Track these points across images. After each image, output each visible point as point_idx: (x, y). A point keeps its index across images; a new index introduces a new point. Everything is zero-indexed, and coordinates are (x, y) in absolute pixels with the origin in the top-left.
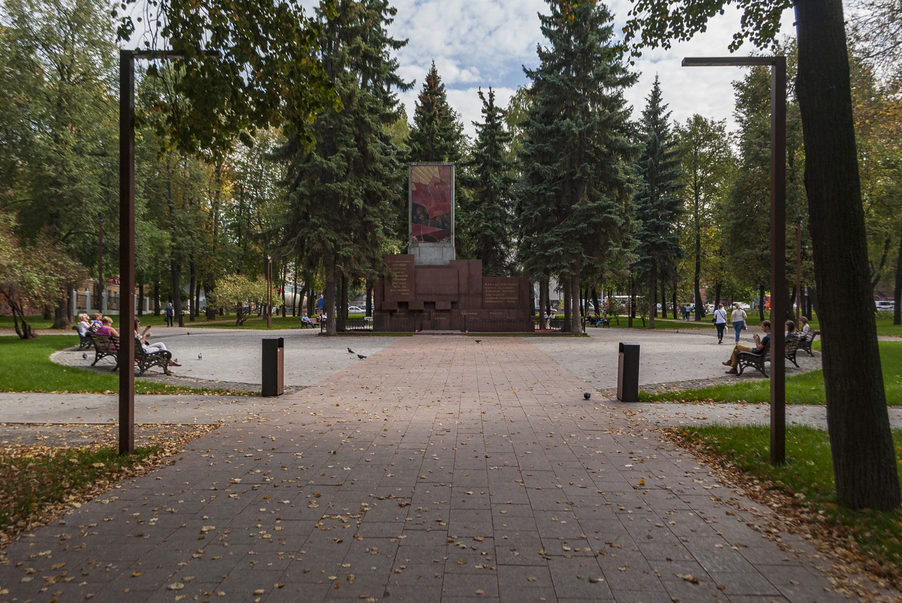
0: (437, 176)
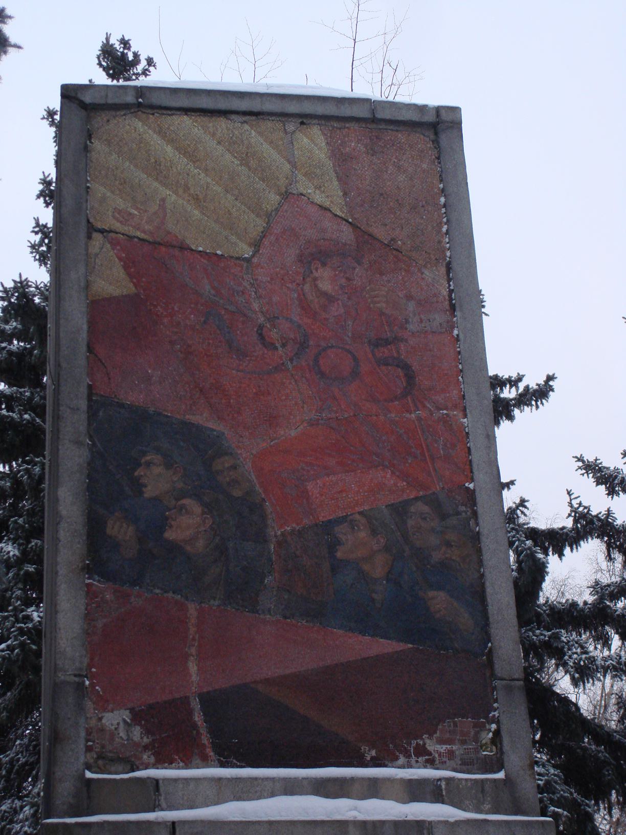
0: (327, 193)
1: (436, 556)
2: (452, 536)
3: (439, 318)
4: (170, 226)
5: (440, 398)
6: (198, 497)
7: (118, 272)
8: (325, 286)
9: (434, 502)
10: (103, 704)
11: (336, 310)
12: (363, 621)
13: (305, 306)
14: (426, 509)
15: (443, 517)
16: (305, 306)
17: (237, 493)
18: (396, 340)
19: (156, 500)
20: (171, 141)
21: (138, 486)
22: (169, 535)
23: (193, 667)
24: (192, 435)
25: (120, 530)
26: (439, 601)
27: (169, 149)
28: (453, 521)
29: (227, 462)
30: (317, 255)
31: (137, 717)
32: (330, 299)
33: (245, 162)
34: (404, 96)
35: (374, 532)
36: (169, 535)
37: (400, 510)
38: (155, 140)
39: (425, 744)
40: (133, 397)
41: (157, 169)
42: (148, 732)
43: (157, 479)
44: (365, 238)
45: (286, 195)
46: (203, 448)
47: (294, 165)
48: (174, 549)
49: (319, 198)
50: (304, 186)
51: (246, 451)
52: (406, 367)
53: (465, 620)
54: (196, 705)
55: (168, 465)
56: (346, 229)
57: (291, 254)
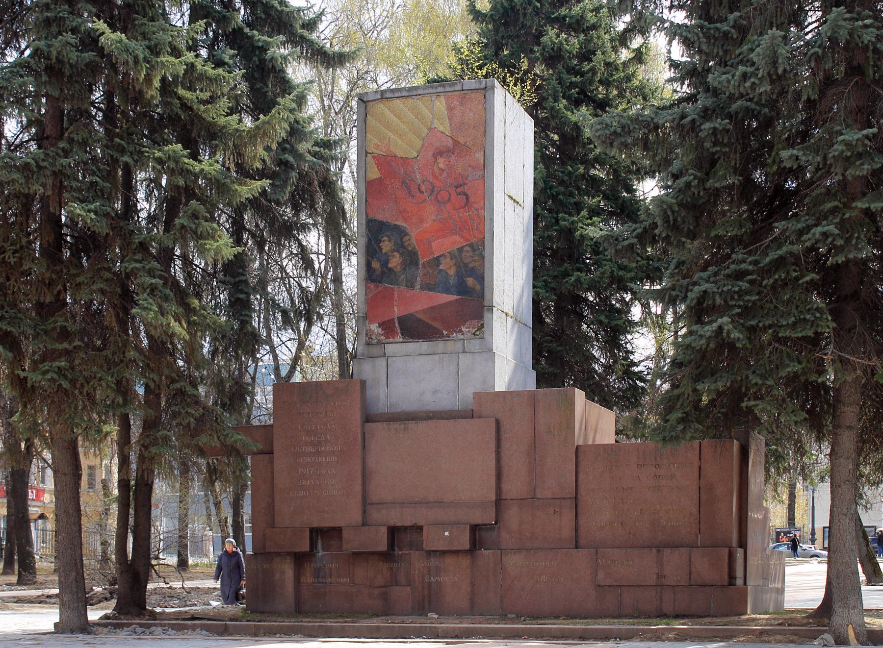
0: (444, 127)
1: (471, 265)
2: (476, 258)
3: (479, 173)
4: (391, 149)
5: (476, 206)
6: (398, 251)
7: (376, 169)
8: (441, 166)
9: (471, 246)
10: (371, 322)
11: (445, 175)
12: (447, 291)
13: (433, 174)
14: (469, 249)
15: (474, 251)
16: (433, 174)
17: (410, 249)
18: (465, 184)
19: (386, 253)
20: (392, 112)
21: (381, 249)
22: (390, 265)
23: (396, 308)
24: (397, 228)
25: (376, 265)
26: (470, 281)
27: (392, 115)
28: (477, 252)
29: (407, 238)
30: (439, 153)
31: (380, 325)
32: (443, 170)
33: (417, 117)
34: (494, 484)
35: (452, 259)
36: (390, 265)
37: (460, 250)
38: (387, 111)
39: (672, 22)
40: (380, 217)
41: (388, 125)
42: (383, 330)
43: (386, 246)
44: (456, 143)
45: (430, 129)
46: (400, 232)
47: (433, 115)
48: (390, 270)
49: (441, 129)
50: (436, 124)
51: (414, 234)
52: (466, 195)
53: (478, 287)
54: (396, 321)
55: (390, 241)
56: (450, 140)
57: (430, 154)
